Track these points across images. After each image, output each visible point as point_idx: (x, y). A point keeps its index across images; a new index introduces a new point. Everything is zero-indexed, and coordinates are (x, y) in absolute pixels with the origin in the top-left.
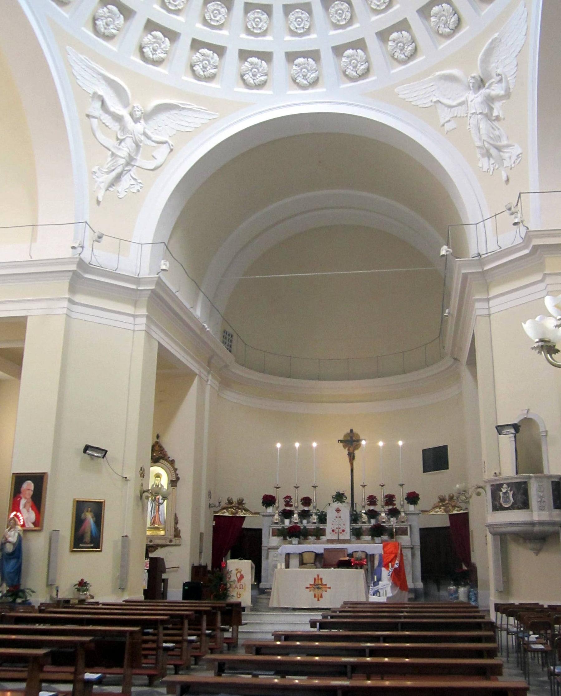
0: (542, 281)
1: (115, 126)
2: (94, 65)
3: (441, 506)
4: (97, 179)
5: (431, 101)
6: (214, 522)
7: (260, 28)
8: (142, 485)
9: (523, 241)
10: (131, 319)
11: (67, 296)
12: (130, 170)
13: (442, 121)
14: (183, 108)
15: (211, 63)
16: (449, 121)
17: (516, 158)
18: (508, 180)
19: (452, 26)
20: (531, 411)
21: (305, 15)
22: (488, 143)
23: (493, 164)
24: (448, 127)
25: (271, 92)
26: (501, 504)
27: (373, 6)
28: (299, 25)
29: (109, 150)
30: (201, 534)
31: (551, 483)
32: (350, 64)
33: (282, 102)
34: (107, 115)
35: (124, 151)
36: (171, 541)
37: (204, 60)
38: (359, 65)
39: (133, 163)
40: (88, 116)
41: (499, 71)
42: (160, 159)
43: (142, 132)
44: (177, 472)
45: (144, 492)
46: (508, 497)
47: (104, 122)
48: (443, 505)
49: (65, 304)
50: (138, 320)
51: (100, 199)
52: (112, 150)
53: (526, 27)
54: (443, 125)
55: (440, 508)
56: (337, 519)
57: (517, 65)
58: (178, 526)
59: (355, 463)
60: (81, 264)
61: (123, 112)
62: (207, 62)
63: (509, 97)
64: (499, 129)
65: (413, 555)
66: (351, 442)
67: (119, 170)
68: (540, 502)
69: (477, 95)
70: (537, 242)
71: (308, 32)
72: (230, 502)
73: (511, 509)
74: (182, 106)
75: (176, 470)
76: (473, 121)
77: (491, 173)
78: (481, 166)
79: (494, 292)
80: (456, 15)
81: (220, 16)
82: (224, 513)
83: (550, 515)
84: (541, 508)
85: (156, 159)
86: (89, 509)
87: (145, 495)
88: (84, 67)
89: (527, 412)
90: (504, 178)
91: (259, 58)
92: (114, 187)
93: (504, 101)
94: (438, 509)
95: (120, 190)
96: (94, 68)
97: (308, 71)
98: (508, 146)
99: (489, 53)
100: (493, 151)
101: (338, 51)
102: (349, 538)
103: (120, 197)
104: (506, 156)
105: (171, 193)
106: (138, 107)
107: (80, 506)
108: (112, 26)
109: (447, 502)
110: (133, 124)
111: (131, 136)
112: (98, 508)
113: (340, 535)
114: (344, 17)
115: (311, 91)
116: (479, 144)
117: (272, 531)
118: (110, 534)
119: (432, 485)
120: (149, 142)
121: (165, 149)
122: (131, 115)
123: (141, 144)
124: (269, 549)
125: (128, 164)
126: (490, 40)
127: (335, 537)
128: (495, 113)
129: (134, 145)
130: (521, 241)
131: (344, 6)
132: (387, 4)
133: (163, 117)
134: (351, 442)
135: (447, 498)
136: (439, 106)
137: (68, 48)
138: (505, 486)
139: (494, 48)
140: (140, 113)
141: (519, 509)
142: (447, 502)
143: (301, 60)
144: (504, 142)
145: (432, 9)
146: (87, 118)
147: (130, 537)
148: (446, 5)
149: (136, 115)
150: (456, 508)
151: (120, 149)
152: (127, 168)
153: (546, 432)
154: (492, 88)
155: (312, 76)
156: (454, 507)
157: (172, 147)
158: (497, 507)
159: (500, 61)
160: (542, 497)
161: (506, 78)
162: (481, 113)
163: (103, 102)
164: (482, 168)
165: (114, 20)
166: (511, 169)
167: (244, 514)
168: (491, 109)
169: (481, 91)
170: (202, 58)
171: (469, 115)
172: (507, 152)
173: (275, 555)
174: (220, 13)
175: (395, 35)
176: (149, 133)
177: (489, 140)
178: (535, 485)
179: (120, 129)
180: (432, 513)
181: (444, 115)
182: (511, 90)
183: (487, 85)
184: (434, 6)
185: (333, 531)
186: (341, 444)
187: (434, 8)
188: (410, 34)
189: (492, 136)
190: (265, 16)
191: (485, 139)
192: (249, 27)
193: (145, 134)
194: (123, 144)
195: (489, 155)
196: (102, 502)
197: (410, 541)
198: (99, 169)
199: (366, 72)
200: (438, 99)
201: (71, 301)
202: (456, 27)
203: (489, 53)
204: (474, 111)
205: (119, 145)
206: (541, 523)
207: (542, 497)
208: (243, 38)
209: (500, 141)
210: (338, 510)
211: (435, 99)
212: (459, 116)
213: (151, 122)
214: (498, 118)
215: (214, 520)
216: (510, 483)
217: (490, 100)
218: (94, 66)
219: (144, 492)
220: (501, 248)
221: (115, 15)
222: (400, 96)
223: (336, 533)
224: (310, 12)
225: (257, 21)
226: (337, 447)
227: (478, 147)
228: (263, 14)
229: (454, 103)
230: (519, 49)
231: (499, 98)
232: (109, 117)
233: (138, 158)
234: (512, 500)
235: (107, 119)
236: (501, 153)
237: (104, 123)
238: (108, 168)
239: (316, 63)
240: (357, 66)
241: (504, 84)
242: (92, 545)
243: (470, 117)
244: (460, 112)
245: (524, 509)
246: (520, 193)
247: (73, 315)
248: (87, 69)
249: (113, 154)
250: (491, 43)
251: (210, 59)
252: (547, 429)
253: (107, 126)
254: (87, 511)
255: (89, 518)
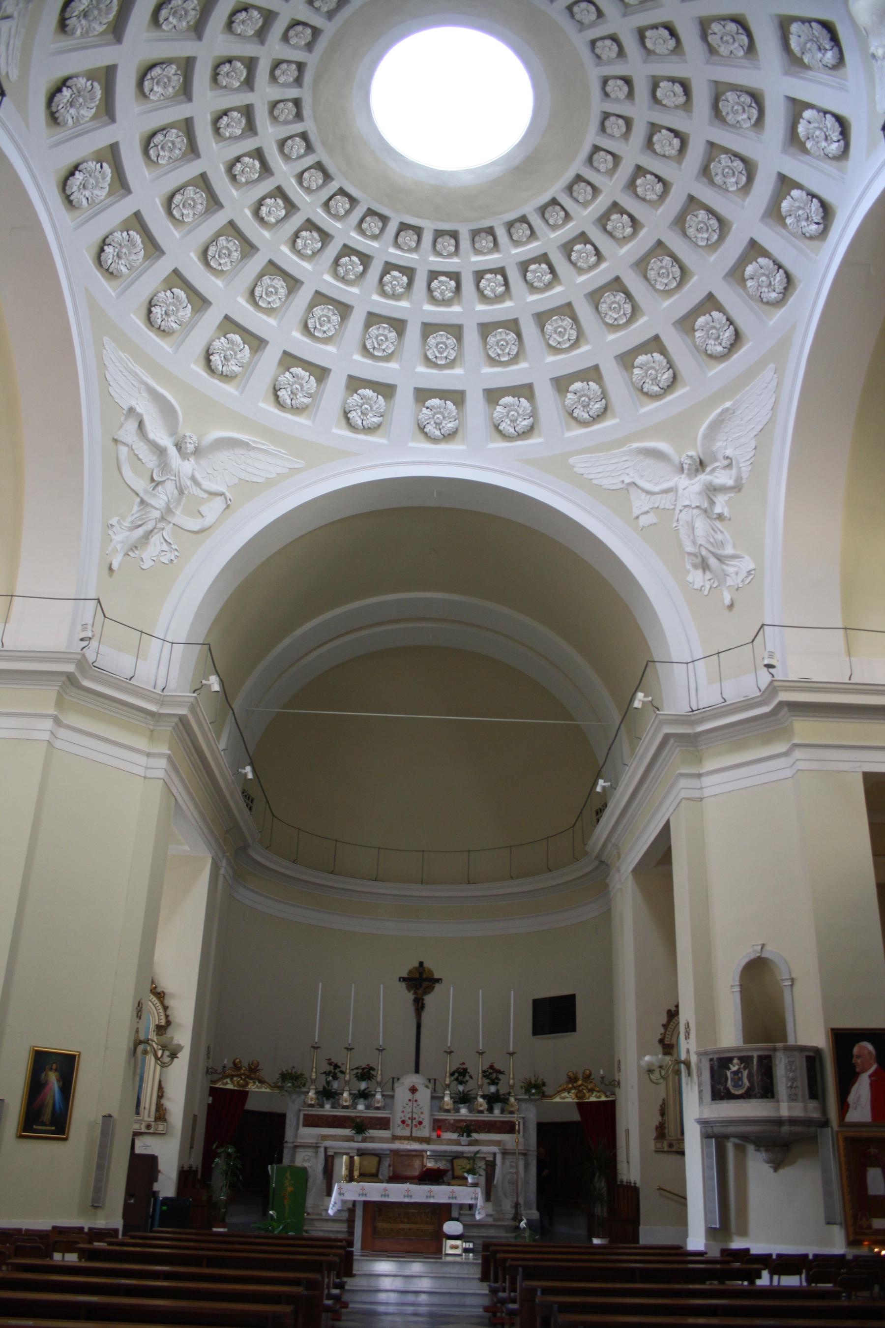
0: (786, 754)
1: (150, 460)
2: (138, 369)
3: (571, 1089)
4: (113, 536)
5: (623, 482)
6: (211, 1098)
7: (384, 350)
8: (137, 1031)
9: (761, 696)
10: (142, 760)
11: (52, 711)
12: (163, 529)
13: (636, 512)
14: (254, 448)
15: (305, 389)
16: (647, 512)
17: (746, 575)
18: (731, 606)
19: (663, 384)
20: (767, 948)
21: (452, 341)
22: (706, 549)
23: (710, 580)
24: (644, 521)
25: (384, 441)
26: (728, 1089)
27: (551, 342)
28: (441, 353)
29: (137, 494)
30: (195, 1116)
31: (804, 1059)
32: (508, 416)
33: (401, 457)
34: (142, 444)
35: (160, 500)
36: (148, 1127)
37: (295, 383)
38: (520, 420)
39: (169, 519)
40: (116, 441)
41: (728, 452)
42: (210, 520)
43: (190, 475)
44: (169, 1012)
45: (141, 1042)
46: (741, 1079)
47: (136, 452)
48: (574, 1088)
49: (49, 724)
50: (153, 762)
51: (115, 566)
52: (142, 494)
53: (773, 400)
54: (637, 518)
55: (569, 1093)
56: (410, 1104)
57: (755, 448)
58: (163, 1101)
59: (425, 1015)
60: (82, 663)
61: (165, 441)
62: (298, 387)
63: (740, 490)
64: (722, 532)
65: (527, 1166)
66: (420, 982)
67: (150, 526)
68: (791, 1087)
69: (692, 482)
70: (784, 696)
71: (451, 364)
72: (236, 1066)
73: (744, 1098)
74: (253, 445)
75: (165, 1008)
76: (684, 516)
77: (706, 593)
78: (691, 581)
79: (709, 765)
80: (671, 370)
81: (329, 325)
82: (227, 1083)
83: (805, 1109)
84: (792, 1098)
85: (203, 517)
86: (54, 1066)
87: (141, 1048)
88: (123, 370)
89: (762, 948)
90: (727, 601)
91: (374, 392)
92: (137, 552)
93: (732, 495)
94: (566, 1094)
95: (144, 557)
96: (137, 374)
97: (444, 418)
98: (734, 557)
99: (716, 425)
100: (713, 561)
101: (493, 396)
102: (427, 1135)
103: (143, 567)
104: (731, 570)
105: (219, 570)
106: (190, 437)
107: (41, 1060)
108: (172, 318)
109: (580, 1082)
110: (179, 460)
111: (173, 478)
112: (67, 1065)
113: (414, 1129)
114: (507, 350)
115: (443, 446)
116: (690, 549)
117: (304, 1118)
118: (85, 1111)
119: (556, 1054)
120: (195, 491)
121: (218, 504)
122: (178, 446)
123: (186, 492)
124: (296, 1147)
125: (163, 518)
126: (719, 410)
127: (406, 1133)
128: (718, 509)
129: (176, 492)
130: (759, 694)
131: (509, 337)
132: (572, 342)
133: (223, 456)
134: (420, 982)
135: (580, 1076)
136: (633, 490)
137: (106, 339)
138: (736, 1061)
139: (723, 421)
140: (192, 446)
141: (755, 1097)
142: (580, 1082)
143: (435, 402)
144: (729, 550)
145: (637, 358)
146: (113, 444)
147: (115, 1115)
148: (659, 355)
149: (186, 449)
150: (595, 1093)
151: (154, 496)
152: (159, 526)
153: (793, 980)
154: (715, 474)
155: (450, 425)
156: (591, 1091)
157: (229, 502)
158: (720, 1093)
159: (730, 439)
160: (793, 1080)
161: (738, 463)
162: (697, 507)
163: (141, 425)
164: (693, 583)
165: (178, 310)
166: (737, 589)
167: (257, 1087)
168: (712, 503)
169: (699, 477)
170: (291, 379)
171: (679, 508)
172: (732, 565)
173: (307, 1158)
174: (329, 321)
175: (577, 385)
176: (198, 476)
177: (708, 546)
178: (783, 1061)
179: (159, 466)
180: (557, 1099)
181: (640, 503)
182: (744, 481)
183: (708, 469)
184: (641, 354)
185: (403, 1122)
186: (403, 985)
187: (640, 357)
188: (601, 387)
189: (712, 540)
190: (393, 335)
191: (703, 543)
192: (368, 347)
193: (193, 479)
194: (160, 488)
195: (704, 566)
196: (74, 1056)
197: (524, 1140)
198: (119, 522)
199: (528, 431)
200: (632, 480)
201: (57, 721)
202: (668, 386)
203: (716, 425)
204: (687, 503)
205: (153, 489)
206: (792, 1121)
207: (793, 1080)
208: (356, 361)
209: (724, 549)
210: (413, 1090)
211: (628, 480)
212: (662, 507)
213: (203, 462)
214: (720, 517)
215: (210, 1095)
216: (744, 1057)
217: (712, 490)
218: (138, 371)
219: (141, 1042)
220: (725, 701)
221: (181, 302)
222: (576, 469)
223: (408, 1125)
224: (459, 338)
225: (382, 340)
226: (417, 984)
227: (689, 554)
228: (391, 332)
229: (657, 489)
230: (759, 427)
231: (723, 489)
232: (146, 447)
233: (178, 512)
234: (746, 1083)
235: (142, 450)
236: (724, 567)
237: (137, 455)
238: (132, 522)
239: (457, 408)
240: (516, 420)
241: (734, 472)
242: (53, 1128)
243: (681, 511)
244: (664, 502)
245: (767, 1097)
246: (763, 625)
247: (58, 744)
248: (126, 374)
249: (142, 501)
250: (721, 414)
251: (304, 382)
252: (793, 976)
253: (140, 459)
254: (51, 1069)
255: (53, 1078)
